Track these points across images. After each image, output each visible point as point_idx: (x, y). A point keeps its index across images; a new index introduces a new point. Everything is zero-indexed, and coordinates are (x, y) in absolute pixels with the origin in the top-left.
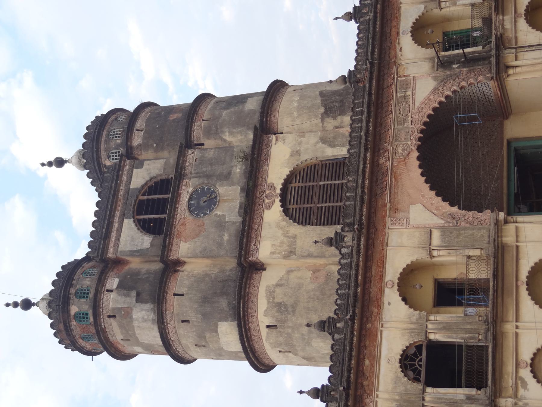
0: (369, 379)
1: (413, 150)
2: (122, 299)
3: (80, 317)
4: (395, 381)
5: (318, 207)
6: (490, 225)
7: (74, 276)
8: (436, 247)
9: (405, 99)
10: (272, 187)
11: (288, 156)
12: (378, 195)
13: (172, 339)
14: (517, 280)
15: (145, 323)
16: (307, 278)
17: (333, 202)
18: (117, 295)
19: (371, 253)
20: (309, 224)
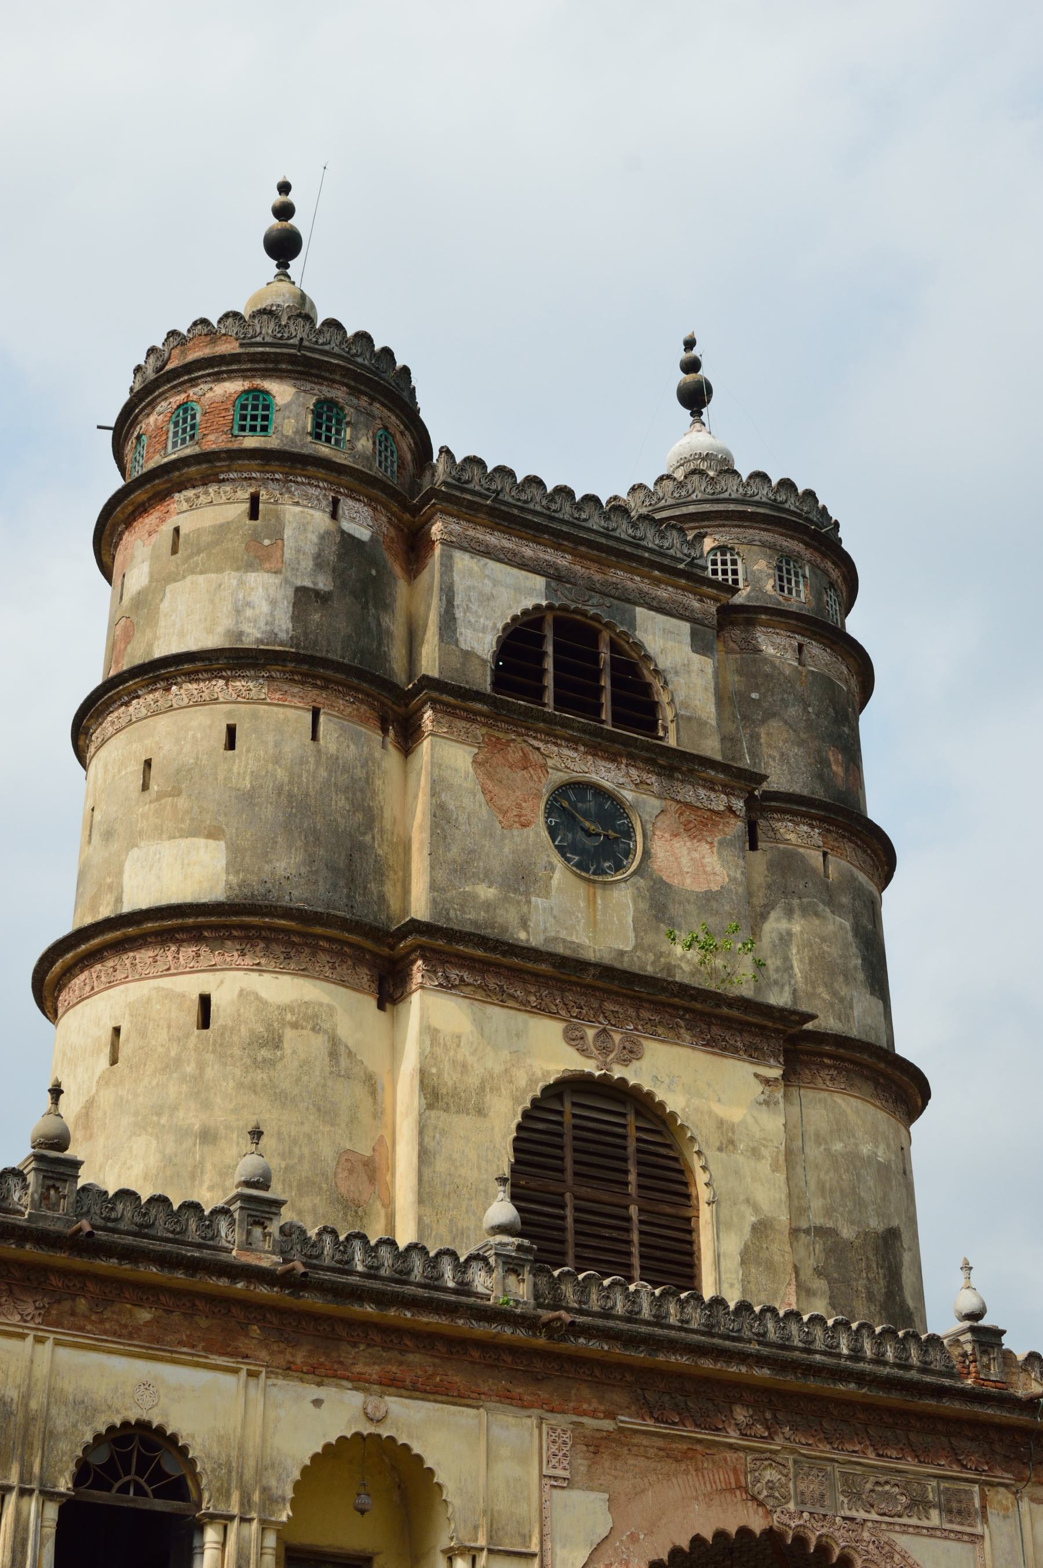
0: (94, 1317)
1: (770, 1519)
2: (310, 542)
3: (255, 408)
4: (83, 1402)
5: (562, 1195)
7: (383, 405)
9: (919, 1504)
10: (631, 1053)
13: (174, 688)
15: (230, 606)
16: (351, 1139)
17: (577, 1245)
18: (322, 531)
20: (517, 1161)
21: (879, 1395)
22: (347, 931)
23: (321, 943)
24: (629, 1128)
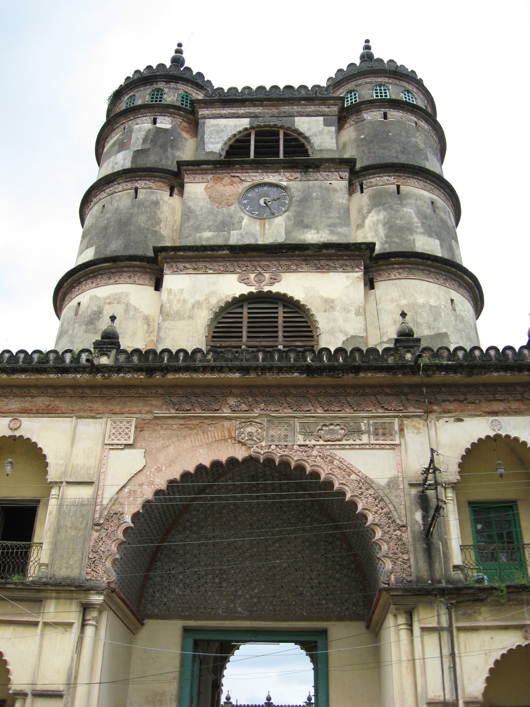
1: (249, 451)
8: (63, 492)
10: (274, 280)
11: (326, 295)
12: (168, 398)
19: (69, 393)
24: (279, 313)
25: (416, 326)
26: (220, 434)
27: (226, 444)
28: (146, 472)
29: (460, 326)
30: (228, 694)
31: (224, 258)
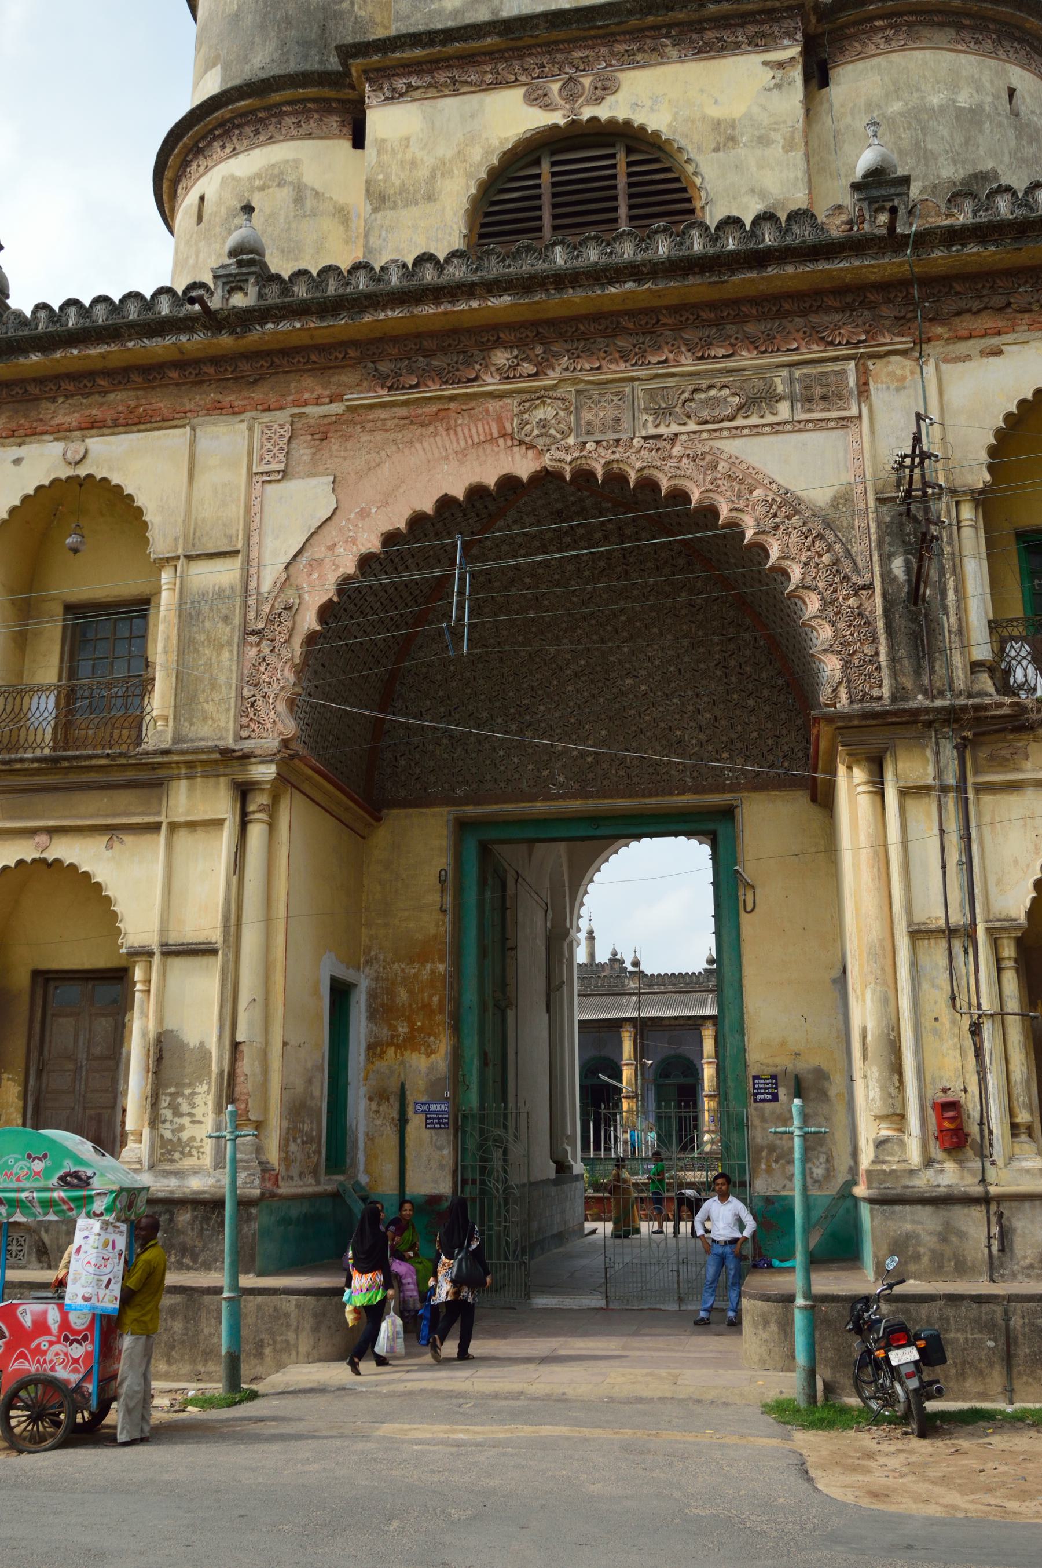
6: (241, 738)
10: (605, 89)
11: (714, 112)
14: (52, 831)
19: (171, 378)
21: (674, 289)
22: (300, 87)
23: (284, 109)
24: (618, 167)
25: (923, 161)
26: (481, 430)
27: (496, 449)
28: (340, 521)
29: (1029, 151)
30: (636, 957)
31: (492, 55)
